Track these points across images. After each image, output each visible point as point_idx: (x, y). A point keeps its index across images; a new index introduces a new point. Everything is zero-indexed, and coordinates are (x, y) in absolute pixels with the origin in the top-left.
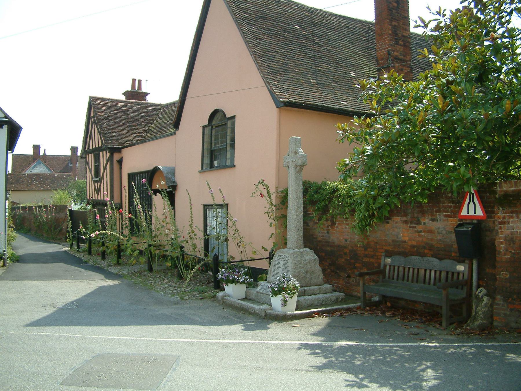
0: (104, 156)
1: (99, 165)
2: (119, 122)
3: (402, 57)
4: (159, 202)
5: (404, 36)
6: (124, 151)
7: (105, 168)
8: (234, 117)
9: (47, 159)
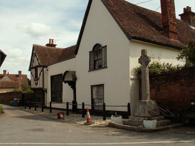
0: (39, 70)
1: (37, 73)
2: (44, 55)
3: (173, 22)
4: (66, 87)
5: (173, 14)
6: (49, 67)
7: (40, 74)
8: (106, 46)
9: (10, 76)
